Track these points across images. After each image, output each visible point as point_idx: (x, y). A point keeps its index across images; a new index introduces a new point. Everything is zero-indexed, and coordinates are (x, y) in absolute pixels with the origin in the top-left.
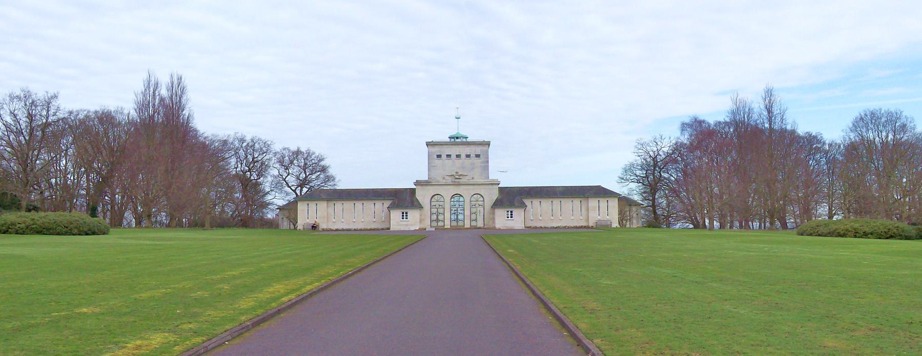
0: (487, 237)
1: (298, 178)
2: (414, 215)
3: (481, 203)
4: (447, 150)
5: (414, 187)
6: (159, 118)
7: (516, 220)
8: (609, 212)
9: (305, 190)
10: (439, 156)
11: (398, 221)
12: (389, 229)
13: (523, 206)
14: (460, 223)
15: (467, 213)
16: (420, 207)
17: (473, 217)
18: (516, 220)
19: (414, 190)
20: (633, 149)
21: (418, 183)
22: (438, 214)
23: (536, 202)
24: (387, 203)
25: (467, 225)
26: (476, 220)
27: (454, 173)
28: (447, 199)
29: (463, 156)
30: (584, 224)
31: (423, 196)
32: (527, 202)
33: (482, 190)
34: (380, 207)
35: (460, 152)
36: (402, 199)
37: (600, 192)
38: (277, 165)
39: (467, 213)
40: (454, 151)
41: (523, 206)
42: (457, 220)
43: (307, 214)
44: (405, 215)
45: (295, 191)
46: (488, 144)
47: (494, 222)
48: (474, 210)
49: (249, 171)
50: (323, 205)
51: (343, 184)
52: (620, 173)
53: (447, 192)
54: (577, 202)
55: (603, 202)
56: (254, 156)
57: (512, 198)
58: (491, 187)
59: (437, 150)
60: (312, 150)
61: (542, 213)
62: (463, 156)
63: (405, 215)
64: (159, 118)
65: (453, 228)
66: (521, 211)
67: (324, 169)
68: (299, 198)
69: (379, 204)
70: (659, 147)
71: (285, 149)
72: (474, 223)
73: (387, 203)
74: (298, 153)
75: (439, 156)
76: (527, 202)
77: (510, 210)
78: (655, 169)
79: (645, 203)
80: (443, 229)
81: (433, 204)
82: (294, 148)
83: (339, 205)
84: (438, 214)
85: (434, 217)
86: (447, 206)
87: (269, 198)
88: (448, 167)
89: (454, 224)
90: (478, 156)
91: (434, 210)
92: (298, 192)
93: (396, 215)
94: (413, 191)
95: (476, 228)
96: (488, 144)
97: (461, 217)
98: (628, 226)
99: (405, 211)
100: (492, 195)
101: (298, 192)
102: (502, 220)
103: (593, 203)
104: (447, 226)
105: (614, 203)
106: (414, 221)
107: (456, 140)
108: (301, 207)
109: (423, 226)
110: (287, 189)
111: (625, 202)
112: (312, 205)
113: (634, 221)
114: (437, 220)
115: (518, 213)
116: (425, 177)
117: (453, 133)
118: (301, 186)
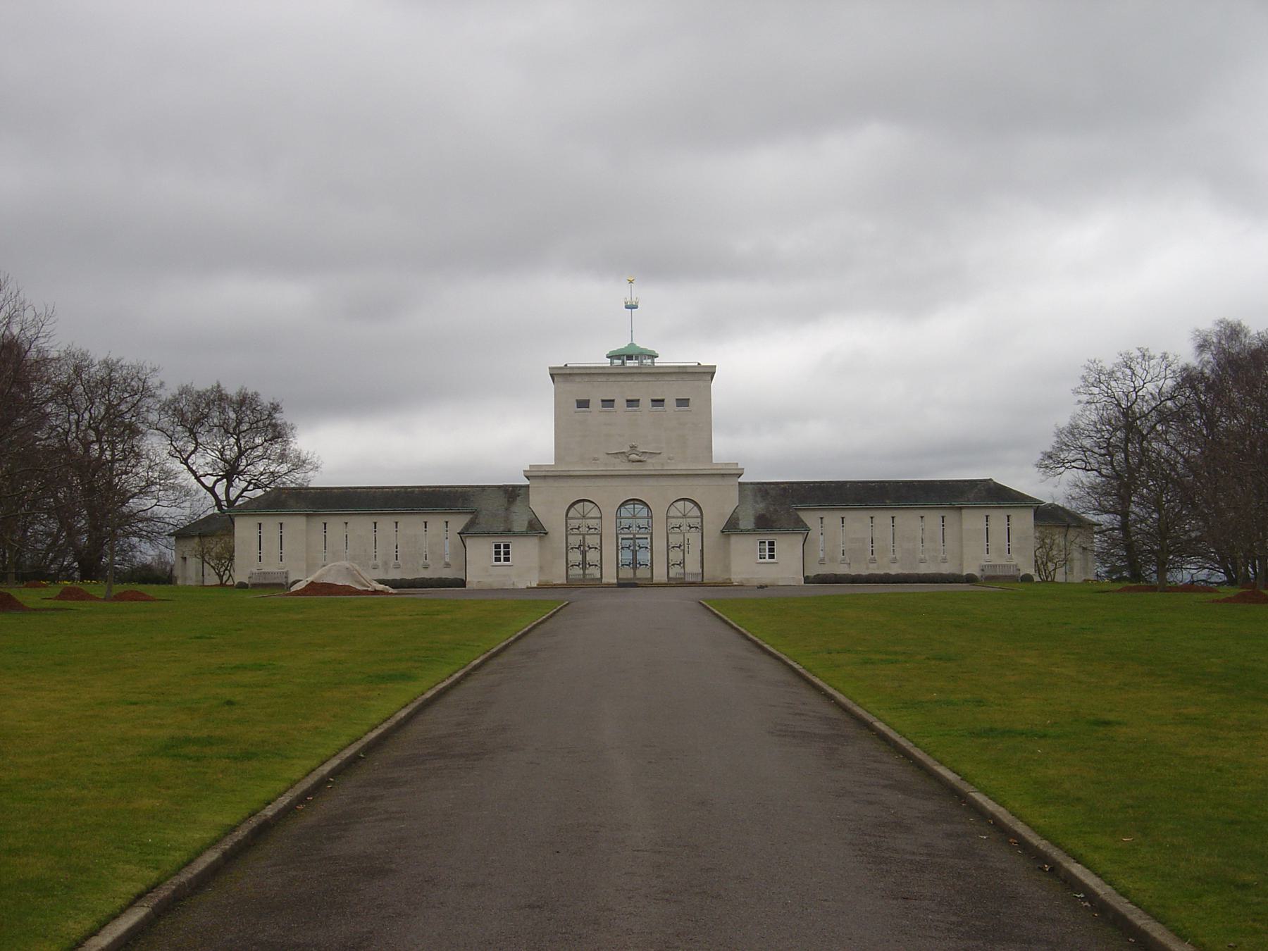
0: (720, 601)
2: (524, 551)
4: (595, 393)
5: (527, 482)
8: (978, 545)
10: (583, 404)
11: (481, 566)
12: (462, 583)
13: (801, 528)
14: (594, 572)
15: (660, 545)
16: (536, 529)
17: (676, 556)
18: (786, 564)
19: (528, 486)
23: (832, 518)
25: (660, 574)
26: (682, 564)
27: (626, 449)
28: (609, 512)
31: (547, 506)
32: (810, 518)
37: (995, 496)
38: (165, 422)
39: (660, 545)
40: (620, 392)
41: (801, 528)
43: (263, 550)
44: (503, 554)
45: (211, 490)
47: (727, 568)
48: (675, 539)
49: (99, 441)
50: (296, 525)
53: (609, 496)
54: (933, 519)
55: (998, 518)
56: (114, 403)
57: (783, 506)
58: (720, 481)
61: (842, 541)
63: (503, 554)
69: (436, 523)
70: (1139, 383)
74: (218, 398)
75: (583, 404)
79: (1104, 519)
83: (336, 525)
86: (609, 529)
89: (627, 573)
90: (683, 402)
91: (575, 540)
92: (220, 489)
93: (480, 552)
94: (512, 494)
97: (592, 556)
99: (502, 541)
100: (721, 503)
101: (220, 489)
102: (746, 563)
103: (973, 520)
105: (1024, 521)
106: (526, 567)
108: (244, 530)
111: (1049, 516)
113: (1077, 565)
114: (584, 564)
115: (789, 547)
117: (621, 344)
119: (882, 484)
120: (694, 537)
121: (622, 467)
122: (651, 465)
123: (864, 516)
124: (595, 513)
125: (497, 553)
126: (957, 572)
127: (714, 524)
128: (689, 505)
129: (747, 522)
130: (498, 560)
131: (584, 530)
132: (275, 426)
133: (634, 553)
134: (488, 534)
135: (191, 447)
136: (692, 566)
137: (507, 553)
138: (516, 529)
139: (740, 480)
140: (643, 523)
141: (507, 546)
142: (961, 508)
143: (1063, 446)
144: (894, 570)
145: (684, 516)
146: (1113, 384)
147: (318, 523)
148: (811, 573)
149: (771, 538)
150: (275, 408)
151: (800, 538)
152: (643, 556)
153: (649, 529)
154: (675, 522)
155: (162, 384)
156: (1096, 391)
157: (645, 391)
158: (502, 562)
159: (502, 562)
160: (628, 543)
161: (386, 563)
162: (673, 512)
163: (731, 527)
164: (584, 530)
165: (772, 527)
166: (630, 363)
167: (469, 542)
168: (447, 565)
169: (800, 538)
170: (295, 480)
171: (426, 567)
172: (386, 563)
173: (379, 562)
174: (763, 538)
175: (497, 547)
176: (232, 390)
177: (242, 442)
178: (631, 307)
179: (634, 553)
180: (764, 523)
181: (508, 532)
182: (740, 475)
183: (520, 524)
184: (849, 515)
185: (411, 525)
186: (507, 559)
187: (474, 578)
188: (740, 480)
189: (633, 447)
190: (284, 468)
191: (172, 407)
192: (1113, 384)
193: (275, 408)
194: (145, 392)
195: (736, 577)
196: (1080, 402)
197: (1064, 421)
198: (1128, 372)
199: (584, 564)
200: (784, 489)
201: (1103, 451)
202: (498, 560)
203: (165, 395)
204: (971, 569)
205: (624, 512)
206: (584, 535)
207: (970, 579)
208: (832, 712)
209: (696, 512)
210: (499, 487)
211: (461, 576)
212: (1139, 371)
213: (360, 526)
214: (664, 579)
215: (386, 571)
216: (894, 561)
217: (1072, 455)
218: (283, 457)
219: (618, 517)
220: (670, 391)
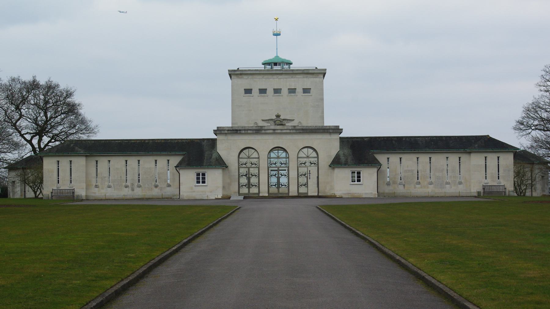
0: (342, 214)
1: (35, 121)
2: (214, 177)
3: (312, 160)
4: (257, 84)
5: (214, 137)
6: (347, 151)
7: (366, 185)
9: (46, 139)
10: (248, 91)
15: (293, 174)
16: (220, 164)
17: (303, 180)
18: (366, 185)
19: (215, 140)
20: (539, 80)
21: (219, 131)
22: (248, 176)
23: (394, 158)
24: (175, 160)
25: (293, 191)
26: (306, 185)
27: (274, 117)
29: (299, 90)
31: (227, 149)
32: (382, 158)
33: (315, 140)
34: (164, 166)
35: (69, 94)
36: (195, 154)
37: (487, 144)
39: (293, 174)
40: (271, 83)
41: (374, 163)
42: (278, 185)
44: (201, 179)
45: (30, 142)
46: (323, 73)
48: (303, 170)
50: (79, 162)
51: (103, 134)
52: (519, 114)
55: (492, 158)
57: (361, 152)
59: (246, 82)
60: (55, 80)
62: (299, 90)
63: (201, 179)
65: (271, 197)
67: (72, 109)
69: (162, 161)
71: (13, 80)
72: (303, 190)
73: (175, 160)
74: (34, 86)
75: (248, 91)
76: (382, 158)
77: (356, 170)
80: (257, 197)
81: (243, 161)
82: (27, 78)
83: (103, 162)
84: (248, 176)
85: (274, 180)
86: (263, 164)
88: (263, 110)
89: (274, 190)
90: (306, 91)
91: (243, 171)
92: (35, 141)
93: (188, 176)
94: (212, 142)
95: (306, 196)
96: (323, 73)
98: (528, 194)
99: (201, 171)
100: (329, 148)
101: (35, 141)
102: (342, 184)
104: (264, 192)
105: (508, 160)
106: (213, 186)
107: (276, 67)
109: (227, 193)
110: (17, 138)
112: (64, 162)
115: (369, 175)
116: (227, 123)
117: (270, 56)
118: (40, 132)
120: (313, 169)
123: (413, 157)
124: (255, 155)
125: (198, 179)
128: (311, 151)
130: (198, 182)
131: (249, 165)
133: (249, 179)
137: (204, 178)
139: (341, 135)
141: (204, 174)
142: (470, 153)
145: (308, 157)
147: (92, 161)
151: (375, 170)
154: (303, 160)
157: (285, 83)
158: (201, 184)
159: (201, 184)
160: (274, 173)
161: (133, 184)
162: (301, 154)
164: (249, 165)
166: (275, 68)
169: (375, 170)
175: (198, 174)
176: (42, 81)
178: (277, 35)
179: (278, 178)
184: (143, 160)
202: (198, 182)
205: (242, 155)
206: (249, 168)
209: (314, 154)
214: (296, 194)
219: (269, 158)
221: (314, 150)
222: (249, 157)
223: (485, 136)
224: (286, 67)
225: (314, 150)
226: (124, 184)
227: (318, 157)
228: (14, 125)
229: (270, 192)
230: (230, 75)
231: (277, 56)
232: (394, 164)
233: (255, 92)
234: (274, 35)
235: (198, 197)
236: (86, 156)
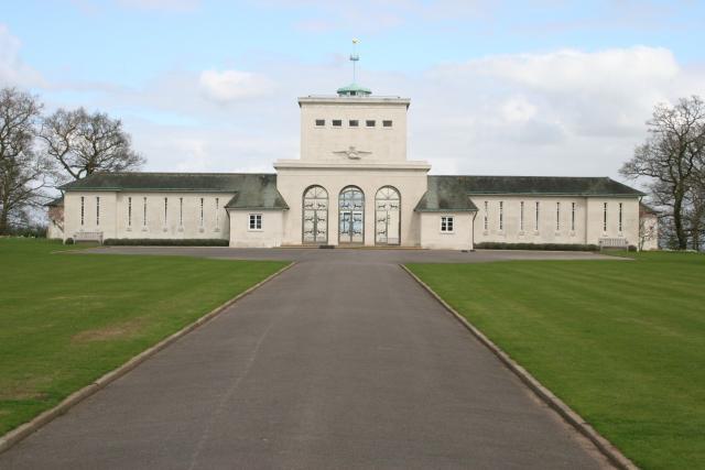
0: (421, 268)
2: (270, 219)
4: (329, 114)
5: (274, 171)
6: (445, 193)
10: (320, 123)
11: (242, 233)
13: (472, 209)
14: (357, 238)
15: (369, 219)
16: (281, 205)
18: (463, 235)
19: (275, 175)
22: (316, 220)
23: (494, 203)
24: (225, 199)
26: (385, 232)
28: (334, 194)
29: (345, 123)
30: (576, 240)
31: (289, 188)
32: (478, 202)
34: (214, 205)
36: (250, 192)
38: (46, 130)
40: (345, 114)
41: (472, 209)
42: (351, 232)
44: (255, 223)
48: (381, 215)
50: (108, 199)
51: (152, 166)
52: (621, 166)
54: (566, 204)
55: (613, 205)
57: (458, 193)
63: (255, 223)
64: (445, 193)
66: (469, 217)
67: (120, 141)
68: (68, 188)
69: (210, 200)
73: (225, 199)
74: (82, 117)
75: (320, 123)
76: (478, 202)
78: (681, 155)
84: (316, 220)
85: (309, 226)
86: (334, 206)
87: (32, 185)
90: (387, 123)
91: (310, 214)
93: (240, 220)
94: (268, 180)
97: (321, 226)
99: (256, 214)
100: (415, 189)
102: (432, 234)
103: (595, 206)
104: (333, 241)
106: (277, 232)
112: (90, 199)
114: (315, 231)
115: (461, 221)
117: (345, 86)
119: (518, 179)
120: (394, 215)
121: (345, 162)
122: (364, 162)
124: (324, 195)
125: (252, 222)
126: (583, 243)
127: (410, 204)
128: (392, 191)
129: (433, 203)
131: (315, 207)
132: (117, 135)
133: (351, 223)
134: (244, 208)
135: (64, 148)
136: (393, 235)
137: (259, 222)
138: (266, 205)
139: (429, 173)
140: (359, 203)
141: (259, 217)
142: (586, 198)
143: (640, 159)
144: (538, 241)
145: (388, 199)
146: (673, 119)
147: (125, 198)
148: (477, 242)
149: (450, 215)
150: (119, 123)
151: (471, 217)
152: (358, 226)
153: (363, 207)
154: (382, 203)
155: (42, 106)
156: (661, 123)
157: (362, 114)
158: (256, 229)
159: (256, 229)
160: (347, 217)
161: (173, 228)
162: (380, 195)
163: (421, 208)
164: (315, 207)
165: (209, 187)
167: (232, 214)
168: (217, 230)
169: (471, 217)
170: (133, 169)
171: (202, 231)
172: (173, 228)
173: (168, 226)
174: (444, 215)
175: (252, 217)
176: (91, 113)
177: (97, 145)
179: (351, 223)
180: (444, 205)
181: (261, 207)
182: (428, 170)
183: (270, 200)
185: (192, 201)
186: (259, 227)
187: (235, 242)
188: (429, 173)
189: (352, 148)
190: (124, 163)
191: (51, 122)
192: (673, 119)
193: (119, 123)
194: (31, 111)
195: (424, 244)
196: (650, 130)
197: (641, 143)
198: (684, 112)
199: (315, 231)
200: (460, 181)
201: (664, 164)
202: (252, 227)
203: (48, 113)
204: (593, 241)
205: (308, 195)
207: (593, 249)
208: (463, 328)
209: (396, 196)
210: (256, 175)
211: (226, 238)
212: (692, 111)
213: (155, 201)
214: (373, 244)
215: (173, 233)
216: (538, 234)
217: (643, 166)
218: (124, 156)
220: (379, 115)
221: (396, 190)
222: (316, 198)
223: (605, 178)
224: (364, 96)
225: (396, 190)
226: (199, 227)
227: (363, 199)
228: (61, 158)
229: (378, 240)
230: (300, 104)
231: (352, 85)
232: (488, 206)
233: (379, 124)
234: (351, 59)
235: (251, 246)
236: (118, 192)
